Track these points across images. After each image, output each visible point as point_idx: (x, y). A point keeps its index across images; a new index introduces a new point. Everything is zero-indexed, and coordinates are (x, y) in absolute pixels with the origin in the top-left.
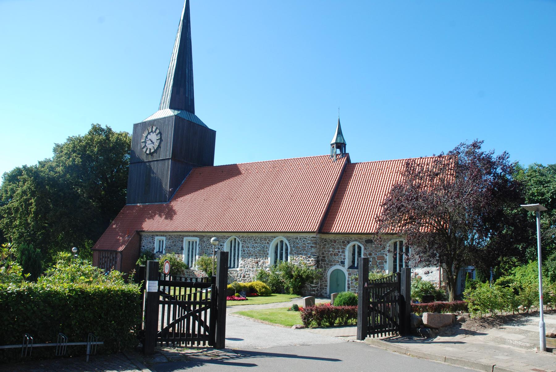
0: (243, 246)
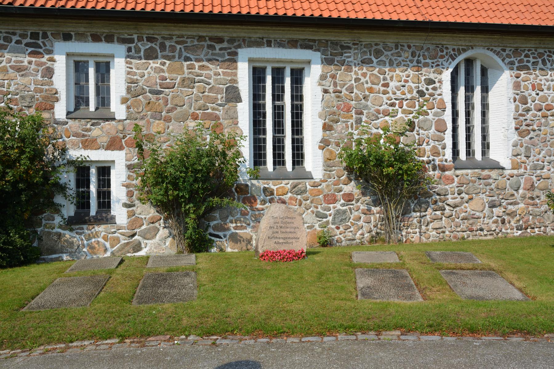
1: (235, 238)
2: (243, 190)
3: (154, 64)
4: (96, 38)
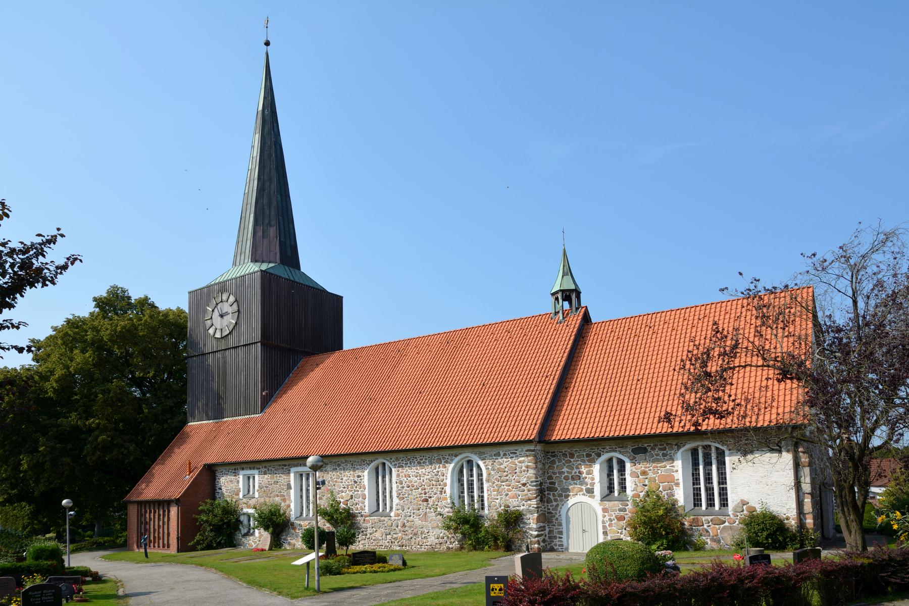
0: (398, 476)
1: (289, 544)
2: (293, 524)
3: (266, 476)
4: (250, 469)
